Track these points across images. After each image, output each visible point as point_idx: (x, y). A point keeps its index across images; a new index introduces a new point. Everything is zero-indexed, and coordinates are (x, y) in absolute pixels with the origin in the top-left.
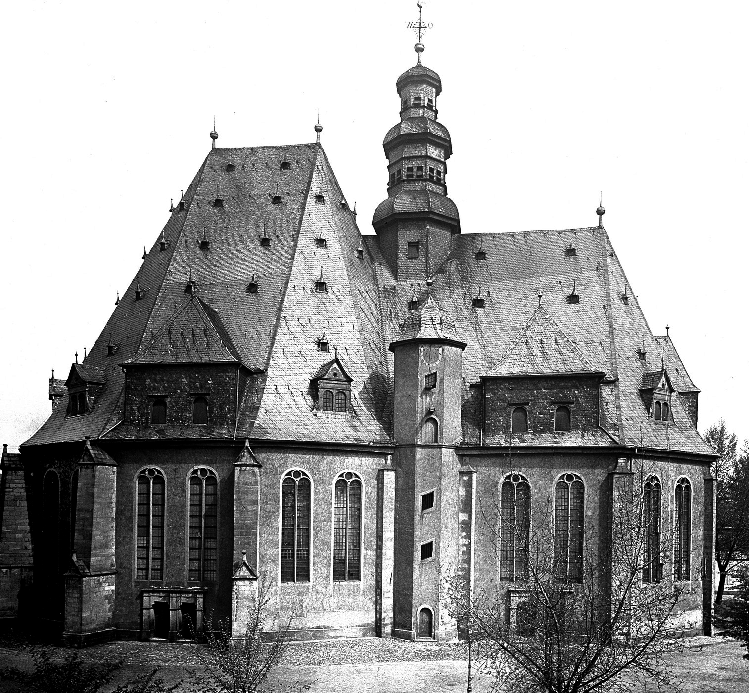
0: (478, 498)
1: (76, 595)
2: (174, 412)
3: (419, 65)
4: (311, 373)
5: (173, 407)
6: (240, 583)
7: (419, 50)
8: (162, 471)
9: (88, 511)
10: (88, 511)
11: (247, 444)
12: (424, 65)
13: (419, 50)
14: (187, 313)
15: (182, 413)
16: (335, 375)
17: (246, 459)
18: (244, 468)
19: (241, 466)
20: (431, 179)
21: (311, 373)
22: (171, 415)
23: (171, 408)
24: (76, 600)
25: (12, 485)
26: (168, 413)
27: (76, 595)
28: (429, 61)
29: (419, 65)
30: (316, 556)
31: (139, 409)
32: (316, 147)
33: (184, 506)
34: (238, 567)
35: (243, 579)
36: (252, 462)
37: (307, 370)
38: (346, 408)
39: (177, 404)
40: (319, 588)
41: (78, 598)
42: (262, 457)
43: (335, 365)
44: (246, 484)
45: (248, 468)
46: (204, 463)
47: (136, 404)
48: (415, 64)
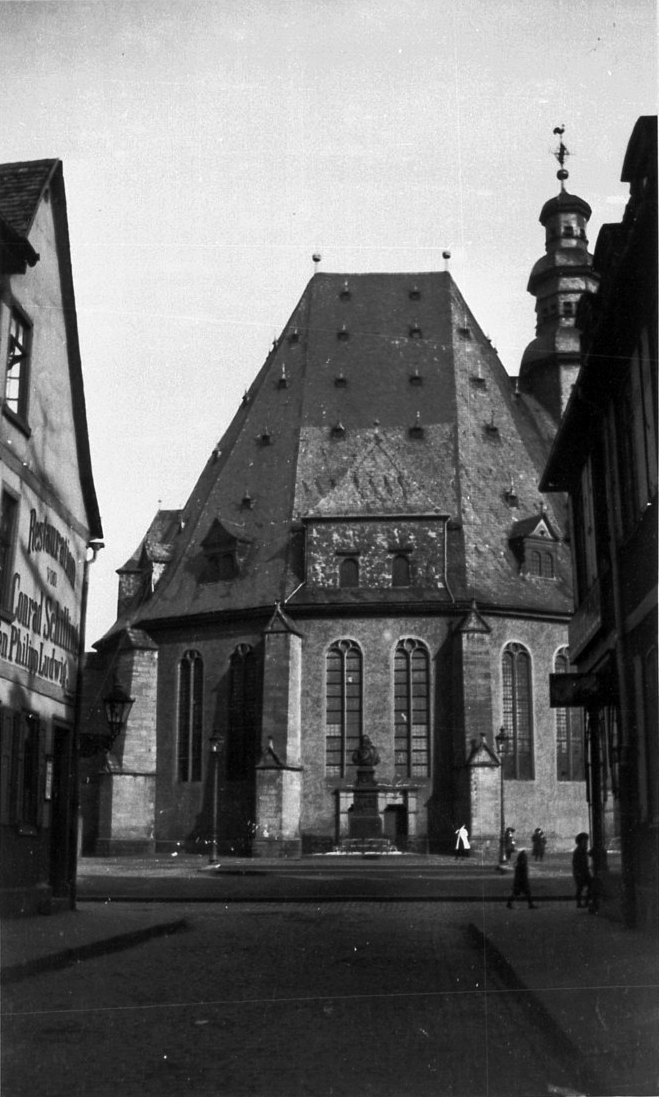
0: (219, 804)
1: (274, 792)
2: (368, 572)
3: (564, 193)
4: (506, 532)
5: (367, 566)
6: (480, 770)
7: (562, 175)
8: (359, 643)
9: (280, 689)
10: (280, 689)
11: (474, 606)
12: (570, 192)
13: (562, 175)
14: (374, 459)
15: (379, 573)
16: (542, 533)
17: (473, 624)
18: (471, 635)
19: (468, 631)
21: (506, 532)
22: (364, 576)
23: (364, 568)
24: (273, 798)
25: (140, 669)
26: (361, 573)
27: (274, 792)
28: (573, 188)
29: (564, 193)
30: (541, 747)
31: (323, 569)
32: (444, 278)
33: (388, 685)
34: (475, 751)
35: (483, 765)
36: (481, 626)
37: (502, 527)
38: (552, 571)
39: (371, 562)
40: (544, 788)
41: (276, 795)
42: (492, 622)
43: (542, 522)
44: (474, 653)
45: (476, 635)
46: (411, 632)
47: (320, 563)
48: (559, 192)
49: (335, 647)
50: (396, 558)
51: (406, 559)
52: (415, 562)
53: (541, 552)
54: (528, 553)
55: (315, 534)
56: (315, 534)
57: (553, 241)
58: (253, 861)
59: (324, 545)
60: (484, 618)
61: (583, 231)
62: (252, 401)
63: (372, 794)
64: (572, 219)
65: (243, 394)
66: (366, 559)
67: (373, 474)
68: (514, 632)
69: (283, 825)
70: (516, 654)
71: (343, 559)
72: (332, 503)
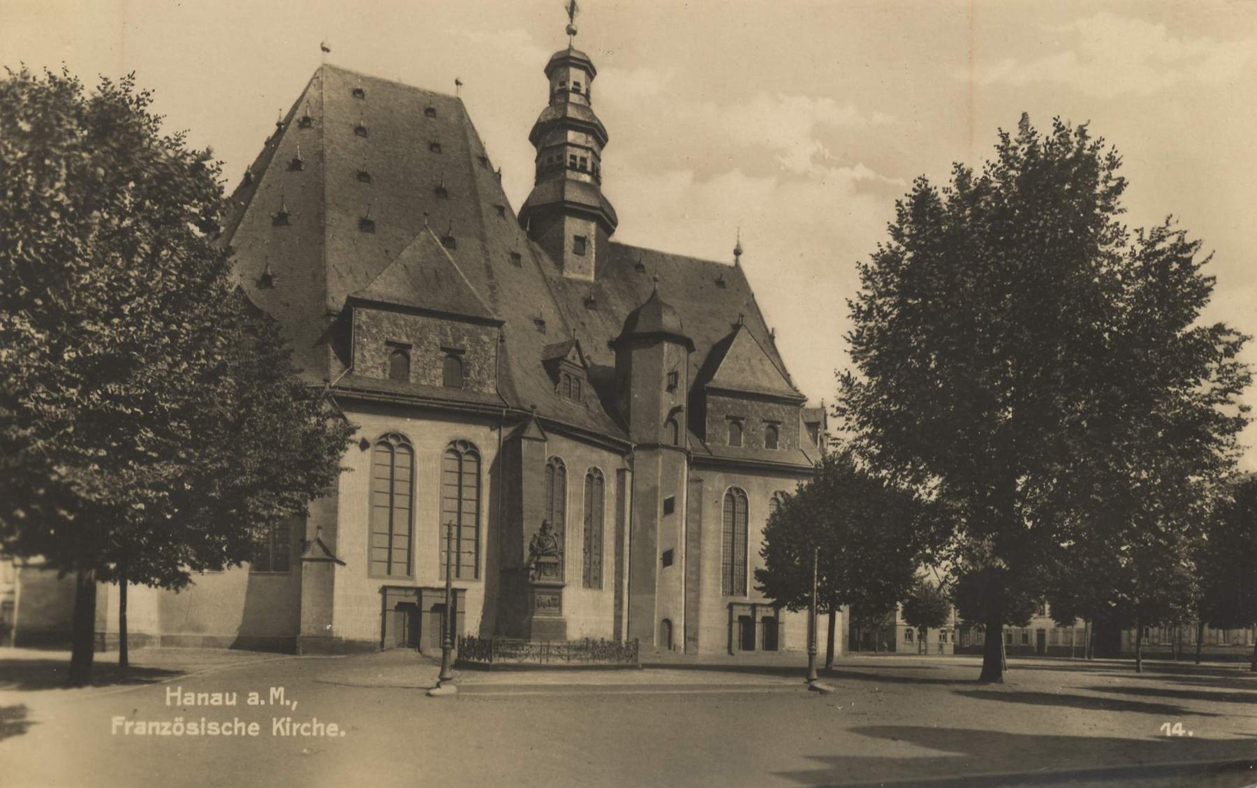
20: (573, 167)
28: (581, 44)
29: (571, 48)
47: (369, 351)
49: (384, 439)
50: (447, 357)
51: (459, 360)
52: (468, 363)
53: (571, 376)
54: (562, 375)
55: (364, 318)
56: (364, 318)
57: (559, 95)
58: (892, 659)
59: (374, 331)
60: (546, 434)
61: (588, 91)
62: (259, 179)
63: (556, 590)
64: (576, 75)
65: (244, 171)
66: (419, 353)
67: (423, 266)
68: (562, 447)
69: (727, 611)
70: (557, 466)
71: (393, 349)
72: (113, 352)
